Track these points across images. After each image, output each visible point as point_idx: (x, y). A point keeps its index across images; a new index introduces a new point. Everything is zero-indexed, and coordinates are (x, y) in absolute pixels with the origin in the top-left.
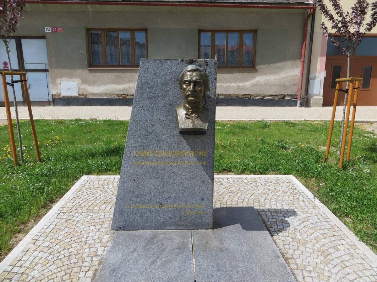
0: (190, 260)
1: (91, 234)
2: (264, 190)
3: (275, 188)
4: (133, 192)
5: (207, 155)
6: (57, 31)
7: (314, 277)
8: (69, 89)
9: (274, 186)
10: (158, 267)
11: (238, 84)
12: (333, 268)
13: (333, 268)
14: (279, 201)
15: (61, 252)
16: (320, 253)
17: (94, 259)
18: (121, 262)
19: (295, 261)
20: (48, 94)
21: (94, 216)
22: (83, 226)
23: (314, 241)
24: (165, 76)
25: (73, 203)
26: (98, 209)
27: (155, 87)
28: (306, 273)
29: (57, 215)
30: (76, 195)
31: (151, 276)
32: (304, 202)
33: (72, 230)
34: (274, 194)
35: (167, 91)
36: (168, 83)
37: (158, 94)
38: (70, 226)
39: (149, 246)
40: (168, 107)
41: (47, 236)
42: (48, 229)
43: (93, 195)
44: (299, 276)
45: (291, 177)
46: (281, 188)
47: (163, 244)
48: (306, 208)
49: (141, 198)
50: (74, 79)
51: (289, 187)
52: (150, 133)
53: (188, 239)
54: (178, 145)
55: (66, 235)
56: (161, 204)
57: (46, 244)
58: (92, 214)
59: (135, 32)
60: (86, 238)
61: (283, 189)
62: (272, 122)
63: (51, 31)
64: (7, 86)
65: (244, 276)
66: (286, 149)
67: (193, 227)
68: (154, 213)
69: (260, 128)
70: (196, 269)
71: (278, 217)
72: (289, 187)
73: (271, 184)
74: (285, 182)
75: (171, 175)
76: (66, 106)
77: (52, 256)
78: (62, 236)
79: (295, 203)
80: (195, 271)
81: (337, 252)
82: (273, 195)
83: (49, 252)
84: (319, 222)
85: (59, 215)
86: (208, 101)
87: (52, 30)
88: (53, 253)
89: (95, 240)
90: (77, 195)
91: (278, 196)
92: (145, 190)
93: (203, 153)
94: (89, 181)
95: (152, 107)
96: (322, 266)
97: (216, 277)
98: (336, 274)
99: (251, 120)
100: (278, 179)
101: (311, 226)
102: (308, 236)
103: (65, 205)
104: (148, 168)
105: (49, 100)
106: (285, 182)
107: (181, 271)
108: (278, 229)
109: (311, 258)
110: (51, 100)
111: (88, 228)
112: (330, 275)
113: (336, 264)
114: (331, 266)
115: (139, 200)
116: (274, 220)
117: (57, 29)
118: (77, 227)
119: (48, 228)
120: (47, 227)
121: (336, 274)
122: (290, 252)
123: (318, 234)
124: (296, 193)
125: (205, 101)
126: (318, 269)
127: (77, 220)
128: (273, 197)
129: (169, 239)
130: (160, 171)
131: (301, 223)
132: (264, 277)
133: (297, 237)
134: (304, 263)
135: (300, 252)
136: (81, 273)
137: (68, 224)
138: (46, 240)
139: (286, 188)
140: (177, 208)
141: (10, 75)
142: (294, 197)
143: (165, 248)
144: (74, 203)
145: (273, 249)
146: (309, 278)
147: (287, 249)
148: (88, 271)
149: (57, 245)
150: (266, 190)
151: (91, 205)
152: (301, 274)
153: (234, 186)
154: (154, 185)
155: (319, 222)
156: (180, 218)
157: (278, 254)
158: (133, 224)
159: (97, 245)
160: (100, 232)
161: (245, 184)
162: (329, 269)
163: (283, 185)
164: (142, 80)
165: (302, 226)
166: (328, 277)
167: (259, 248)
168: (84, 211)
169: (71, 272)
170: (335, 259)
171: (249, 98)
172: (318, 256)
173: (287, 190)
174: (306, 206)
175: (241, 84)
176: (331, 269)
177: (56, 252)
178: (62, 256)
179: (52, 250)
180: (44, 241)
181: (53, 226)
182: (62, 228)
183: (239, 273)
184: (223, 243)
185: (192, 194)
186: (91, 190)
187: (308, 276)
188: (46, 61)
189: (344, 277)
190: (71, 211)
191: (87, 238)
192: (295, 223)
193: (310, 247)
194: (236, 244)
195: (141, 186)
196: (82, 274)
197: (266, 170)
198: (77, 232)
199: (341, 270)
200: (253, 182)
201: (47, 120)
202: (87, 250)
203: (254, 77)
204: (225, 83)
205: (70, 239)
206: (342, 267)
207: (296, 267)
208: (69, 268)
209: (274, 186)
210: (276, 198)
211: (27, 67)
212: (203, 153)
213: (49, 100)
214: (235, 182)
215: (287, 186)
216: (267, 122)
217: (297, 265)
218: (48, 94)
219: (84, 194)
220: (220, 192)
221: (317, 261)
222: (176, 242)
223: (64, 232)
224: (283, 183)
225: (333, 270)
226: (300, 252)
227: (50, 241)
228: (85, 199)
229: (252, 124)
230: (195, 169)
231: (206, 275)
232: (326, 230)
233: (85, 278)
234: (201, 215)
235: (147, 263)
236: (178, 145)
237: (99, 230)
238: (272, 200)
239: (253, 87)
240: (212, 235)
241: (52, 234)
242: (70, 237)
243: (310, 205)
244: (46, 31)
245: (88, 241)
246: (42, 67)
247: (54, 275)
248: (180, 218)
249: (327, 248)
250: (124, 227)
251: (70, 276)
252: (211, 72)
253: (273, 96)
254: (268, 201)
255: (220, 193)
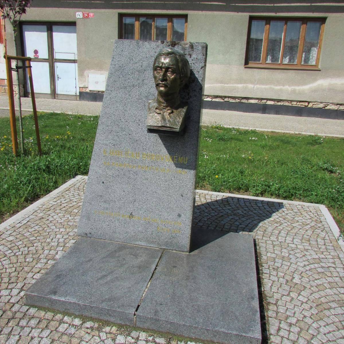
0: (146, 281)
1: (58, 236)
2: (278, 218)
3: (294, 218)
4: (101, 196)
5: (188, 163)
6: (88, 17)
7: (293, 332)
8: (97, 83)
9: (294, 215)
10: (106, 283)
11: (293, 87)
12: (325, 326)
13: (325, 326)
14: (291, 234)
15: (21, 249)
16: (315, 305)
17: (49, 262)
18: (70, 270)
19: (277, 308)
20: (76, 87)
21: (70, 218)
22: (54, 227)
23: (314, 289)
24: (142, 61)
25: (54, 202)
26: (77, 211)
27: (129, 75)
28: (283, 325)
29: (33, 212)
30: (62, 194)
31: (94, 290)
32: (324, 239)
33: (41, 229)
34: (289, 224)
35: (143, 80)
36: (145, 70)
37: (133, 83)
38: (41, 225)
39: (108, 258)
40: (144, 99)
41: (15, 231)
42: (19, 224)
43: (79, 197)
44: (273, 327)
45: (323, 209)
46: (301, 218)
47: (124, 259)
48: (323, 247)
49: (110, 204)
50: (102, 72)
51: (313, 219)
52: (123, 130)
53: (156, 259)
54: (153, 147)
55: (33, 232)
56: (131, 214)
57: (11, 238)
58: (69, 216)
59: (173, 19)
60: (51, 239)
61: (304, 220)
62: (327, 137)
63: (82, 17)
64: (12, 71)
65: (199, 311)
66: (331, 172)
67: (166, 246)
68: (123, 223)
69: (308, 143)
70: (147, 293)
71: (281, 253)
72: (313, 219)
73: (291, 212)
74: (311, 212)
75: (144, 182)
76: (93, 101)
77: (10, 251)
78: (29, 233)
79: (311, 239)
80: (144, 295)
81: (340, 308)
82: (287, 225)
83: (9, 246)
84: (334, 267)
85: (36, 212)
86: (192, 96)
87: (84, 15)
88: (12, 249)
89: (59, 242)
90: (62, 195)
91: (294, 227)
92: (114, 196)
93: (183, 160)
94: (81, 182)
95: (125, 99)
96: (309, 321)
97: (164, 306)
98: (325, 334)
99: (300, 133)
100: (304, 207)
101: (320, 270)
102: (309, 281)
103: (46, 202)
104: (118, 170)
105: (76, 93)
106: (311, 212)
107: (129, 291)
108: (274, 267)
109: (300, 308)
110: (78, 94)
111: (58, 230)
112: (315, 334)
113: (331, 322)
114: (322, 323)
115: (107, 205)
116: (273, 255)
117: (88, 15)
118: (48, 226)
119: (20, 223)
120: (20, 221)
121: (325, 334)
122: (276, 296)
123: (324, 281)
124: (319, 227)
125: (188, 95)
126: (302, 324)
127: (51, 219)
128: (286, 228)
129: (133, 255)
130: (132, 176)
131: (308, 265)
132: (222, 318)
133: (294, 281)
134: (288, 313)
135: (289, 298)
136: (30, 273)
137: (40, 222)
138: (12, 234)
139: (308, 220)
140: (149, 222)
141: (16, 60)
142: (313, 232)
143: (125, 264)
144: (56, 202)
145: (252, 288)
146: (286, 331)
147: (274, 292)
148: (38, 272)
149: (20, 241)
150: (280, 219)
151: (72, 206)
152: (277, 324)
153: (243, 208)
154: (124, 191)
155: (334, 267)
156: (152, 234)
157: (254, 295)
158: (100, 232)
159: (59, 249)
160: (67, 236)
161: (258, 208)
162: (319, 326)
163: (306, 215)
164: (115, 65)
165: (308, 268)
166: (312, 336)
167: (234, 284)
168: (62, 212)
169: (21, 271)
170: (331, 316)
171: (306, 106)
172: (311, 307)
173: (308, 221)
174: (325, 244)
175: (297, 88)
176: (321, 327)
177: (16, 247)
178: (19, 253)
179: (13, 245)
180: (10, 235)
181: (25, 222)
182: (33, 225)
183: (194, 308)
184: (193, 271)
185: (167, 208)
186: (78, 191)
187: (285, 330)
188: (76, 51)
189: (333, 341)
190: (49, 209)
191: (52, 240)
192: (299, 264)
193: (305, 295)
194: (208, 275)
195: (110, 191)
196: (30, 275)
197: (292, 195)
198: (46, 232)
199: (334, 331)
200: (268, 207)
201: (68, 115)
202: (46, 252)
203: (315, 80)
204: (276, 86)
205: (36, 237)
206: (337, 327)
207: (274, 315)
208: (21, 267)
209: (294, 215)
210: (290, 229)
211: (57, 56)
212: (183, 160)
213: (76, 93)
214: (247, 204)
215: (309, 217)
216: (320, 138)
217: (277, 313)
218: (76, 87)
219: (70, 195)
220: (222, 213)
221: (306, 313)
222: (140, 259)
223: (33, 229)
224: (307, 213)
225: (323, 329)
226: (289, 298)
227: (16, 236)
228: (69, 200)
229: (299, 137)
230: (173, 179)
231: (154, 302)
232: (337, 278)
233: (32, 279)
234: (176, 234)
235: (97, 276)
236: (153, 147)
237: (68, 233)
238: (282, 231)
239: (313, 92)
240: (185, 259)
241: (21, 230)
242: (36, 235)
243: (331, 245)
244: (77, 17)
245: (51, 243)
246: (72, 58)
247: (4, 270)
248: (152, 234)
249: (327, 301)
250: (90, 233)
251: (18, 274)
252: (197, 58)
253: (338, 106)
254: (277, 232)
255: (222, 214)
